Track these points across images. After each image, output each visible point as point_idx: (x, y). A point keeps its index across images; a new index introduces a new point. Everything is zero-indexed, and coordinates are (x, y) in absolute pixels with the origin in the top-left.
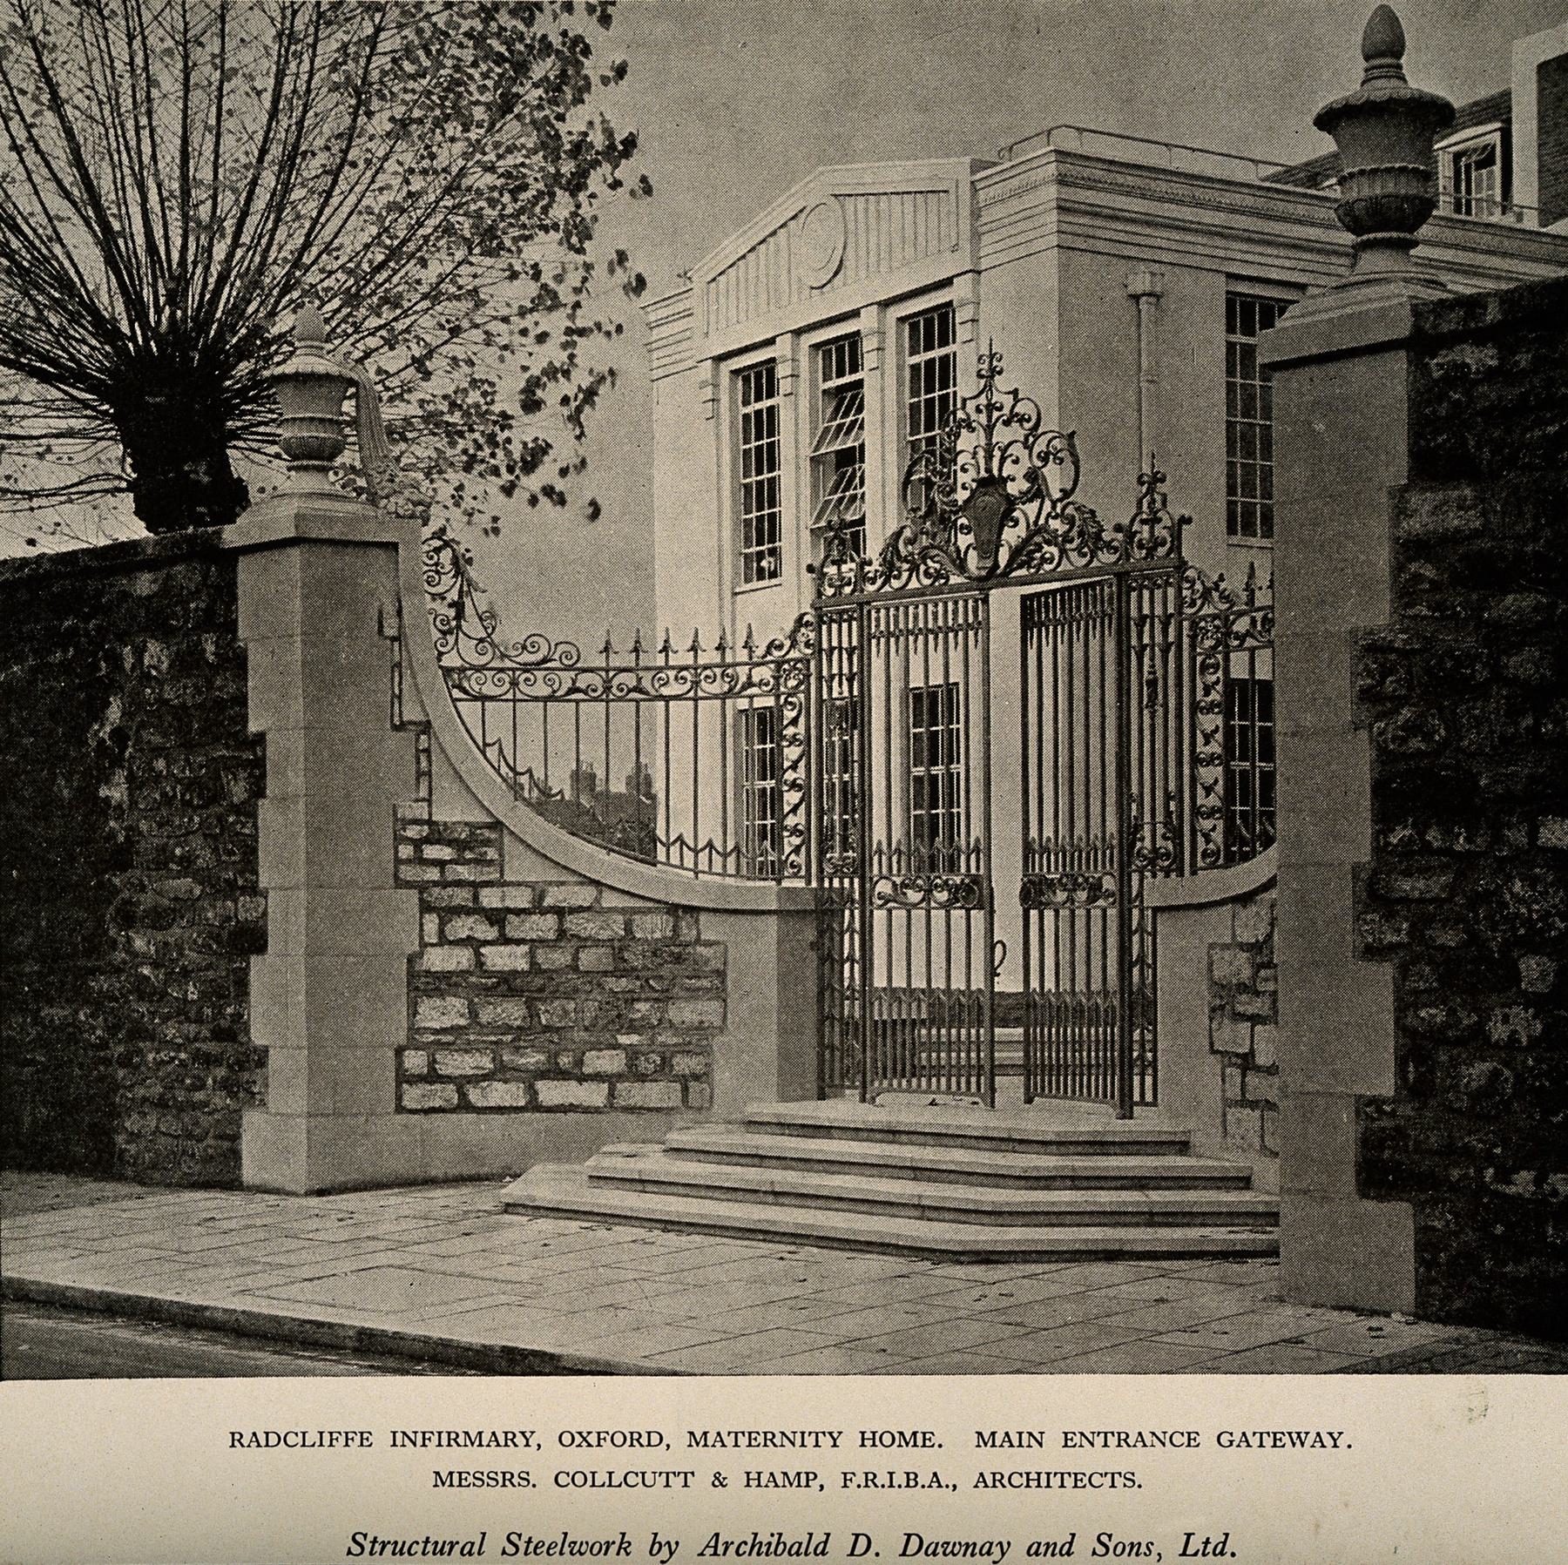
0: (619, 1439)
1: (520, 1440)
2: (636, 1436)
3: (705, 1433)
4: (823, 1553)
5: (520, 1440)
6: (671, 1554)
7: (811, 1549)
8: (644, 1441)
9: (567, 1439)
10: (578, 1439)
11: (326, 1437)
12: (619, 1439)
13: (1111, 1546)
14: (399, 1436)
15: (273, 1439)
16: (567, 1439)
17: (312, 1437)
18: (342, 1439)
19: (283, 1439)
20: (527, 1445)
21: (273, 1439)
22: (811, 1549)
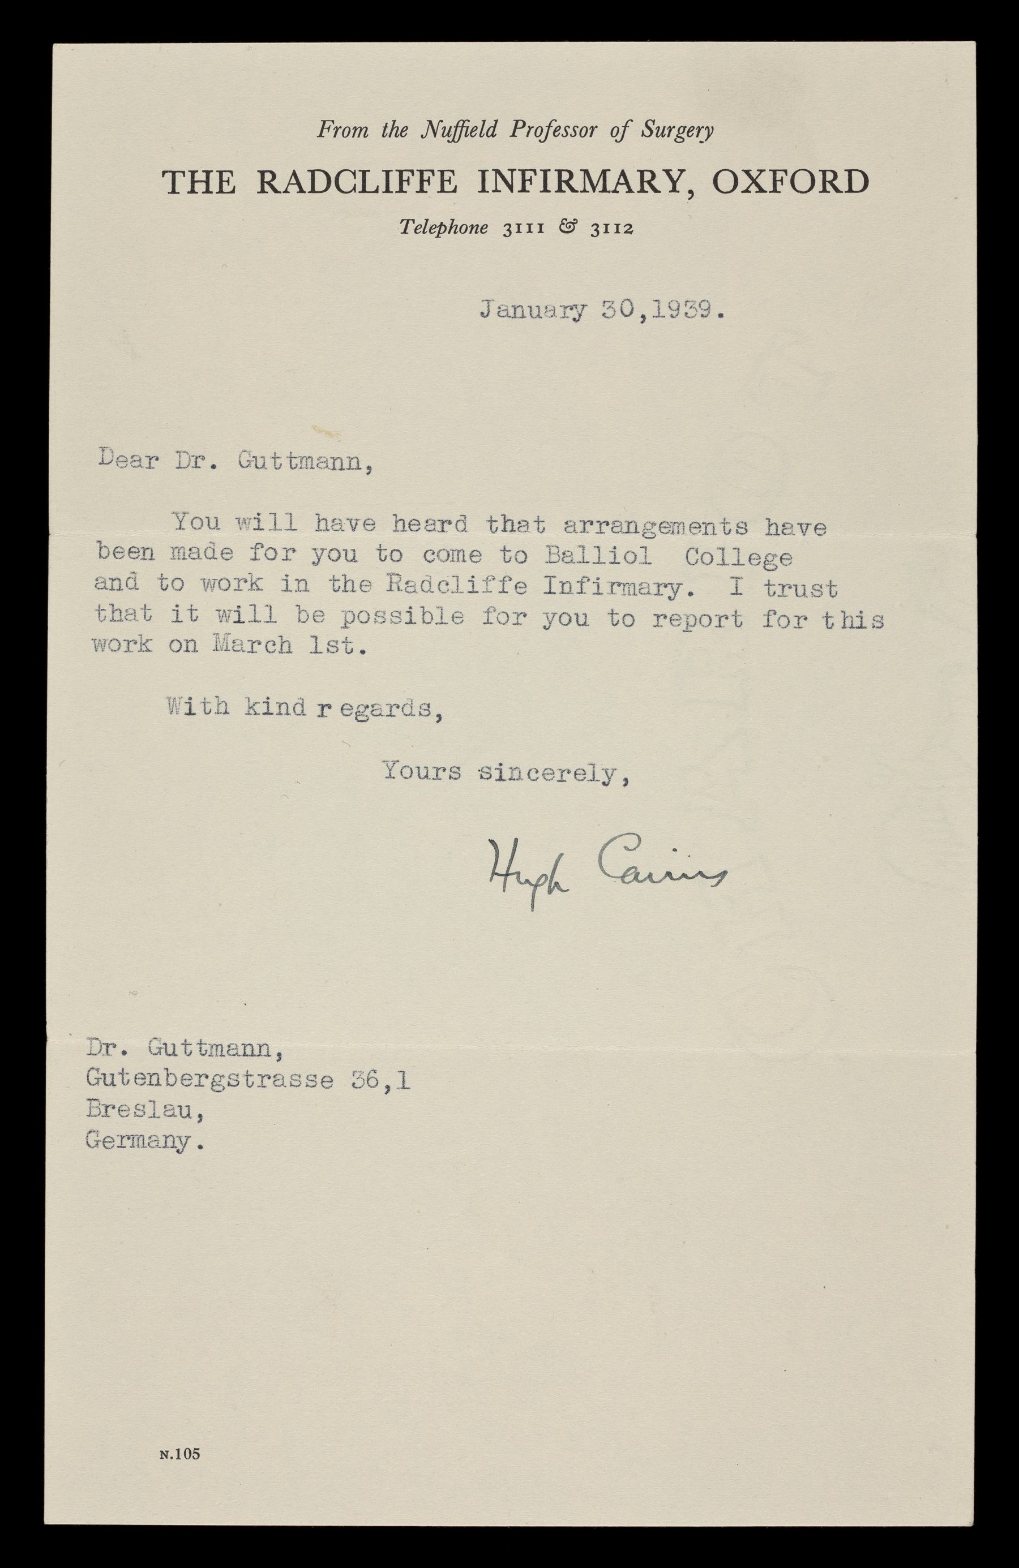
0: (803, 181)
1: (662, 182)
2: (830, 176)
3: (604, 172)
4: (493, 135)
5: (662, 182)
6: (709, 136)
7: (484, 131)
8: (842, 183)
9: (726, 181)
10: (744, 181)
11: (394, 178)
12: (803, 181)
13: (654, 128)
14: (490, 176)
15: (321, 181)
16: (726, 181)
17: (375, 180)
18: (415, 180)
19: (333, 181)
20: (674, 190)
21: (321, 181)
22: (484, 131)
